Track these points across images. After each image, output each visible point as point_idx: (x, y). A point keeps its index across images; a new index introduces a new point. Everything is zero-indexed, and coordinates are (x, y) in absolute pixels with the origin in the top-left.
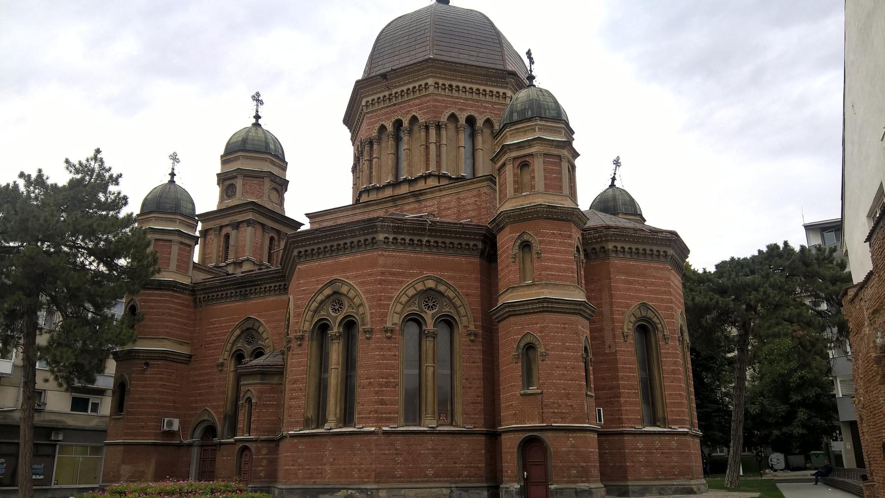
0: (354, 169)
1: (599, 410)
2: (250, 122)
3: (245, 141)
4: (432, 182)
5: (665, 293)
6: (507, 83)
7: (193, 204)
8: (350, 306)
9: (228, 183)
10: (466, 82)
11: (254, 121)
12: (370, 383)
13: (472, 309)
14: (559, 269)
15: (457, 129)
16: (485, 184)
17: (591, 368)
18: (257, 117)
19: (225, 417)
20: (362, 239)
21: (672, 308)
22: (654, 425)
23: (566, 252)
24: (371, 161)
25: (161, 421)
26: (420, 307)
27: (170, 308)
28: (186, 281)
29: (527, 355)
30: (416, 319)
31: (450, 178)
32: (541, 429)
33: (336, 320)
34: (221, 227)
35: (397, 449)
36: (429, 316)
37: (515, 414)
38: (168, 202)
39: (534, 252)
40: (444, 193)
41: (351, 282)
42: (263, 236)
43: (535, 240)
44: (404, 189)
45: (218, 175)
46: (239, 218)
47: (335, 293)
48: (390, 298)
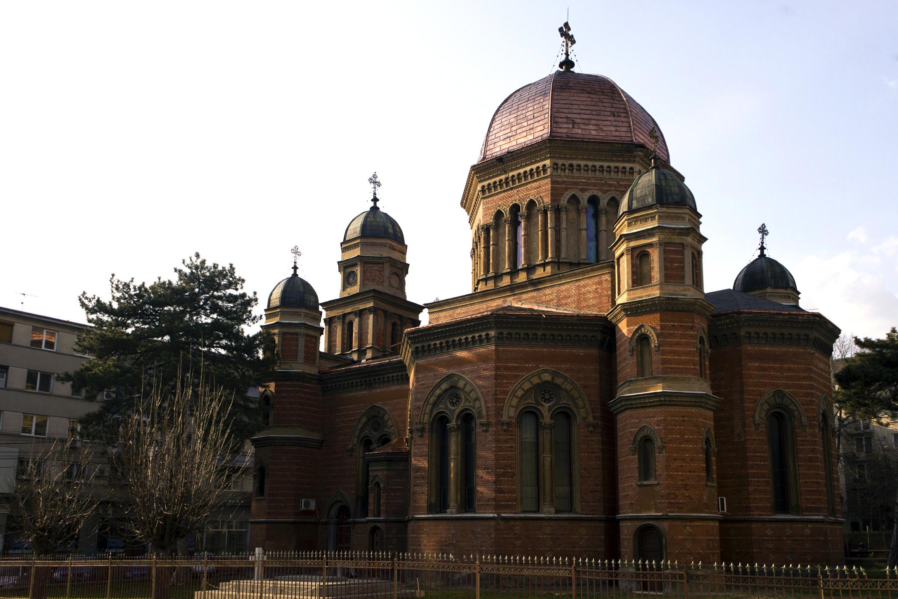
5: (805, 378)
8: (466, 400)
9: (349, 270)
11: (372, 204)
15: (578, 211)
17: (713, 459)
21: (812, 395)
23: (688, 344)
28: (313, 371)
30: (531, 413)
32: (657, 518)
33: (454, 412)
36: (545, 409)
37: (631, 504)
47: (452, 387)
48: (506, 393)
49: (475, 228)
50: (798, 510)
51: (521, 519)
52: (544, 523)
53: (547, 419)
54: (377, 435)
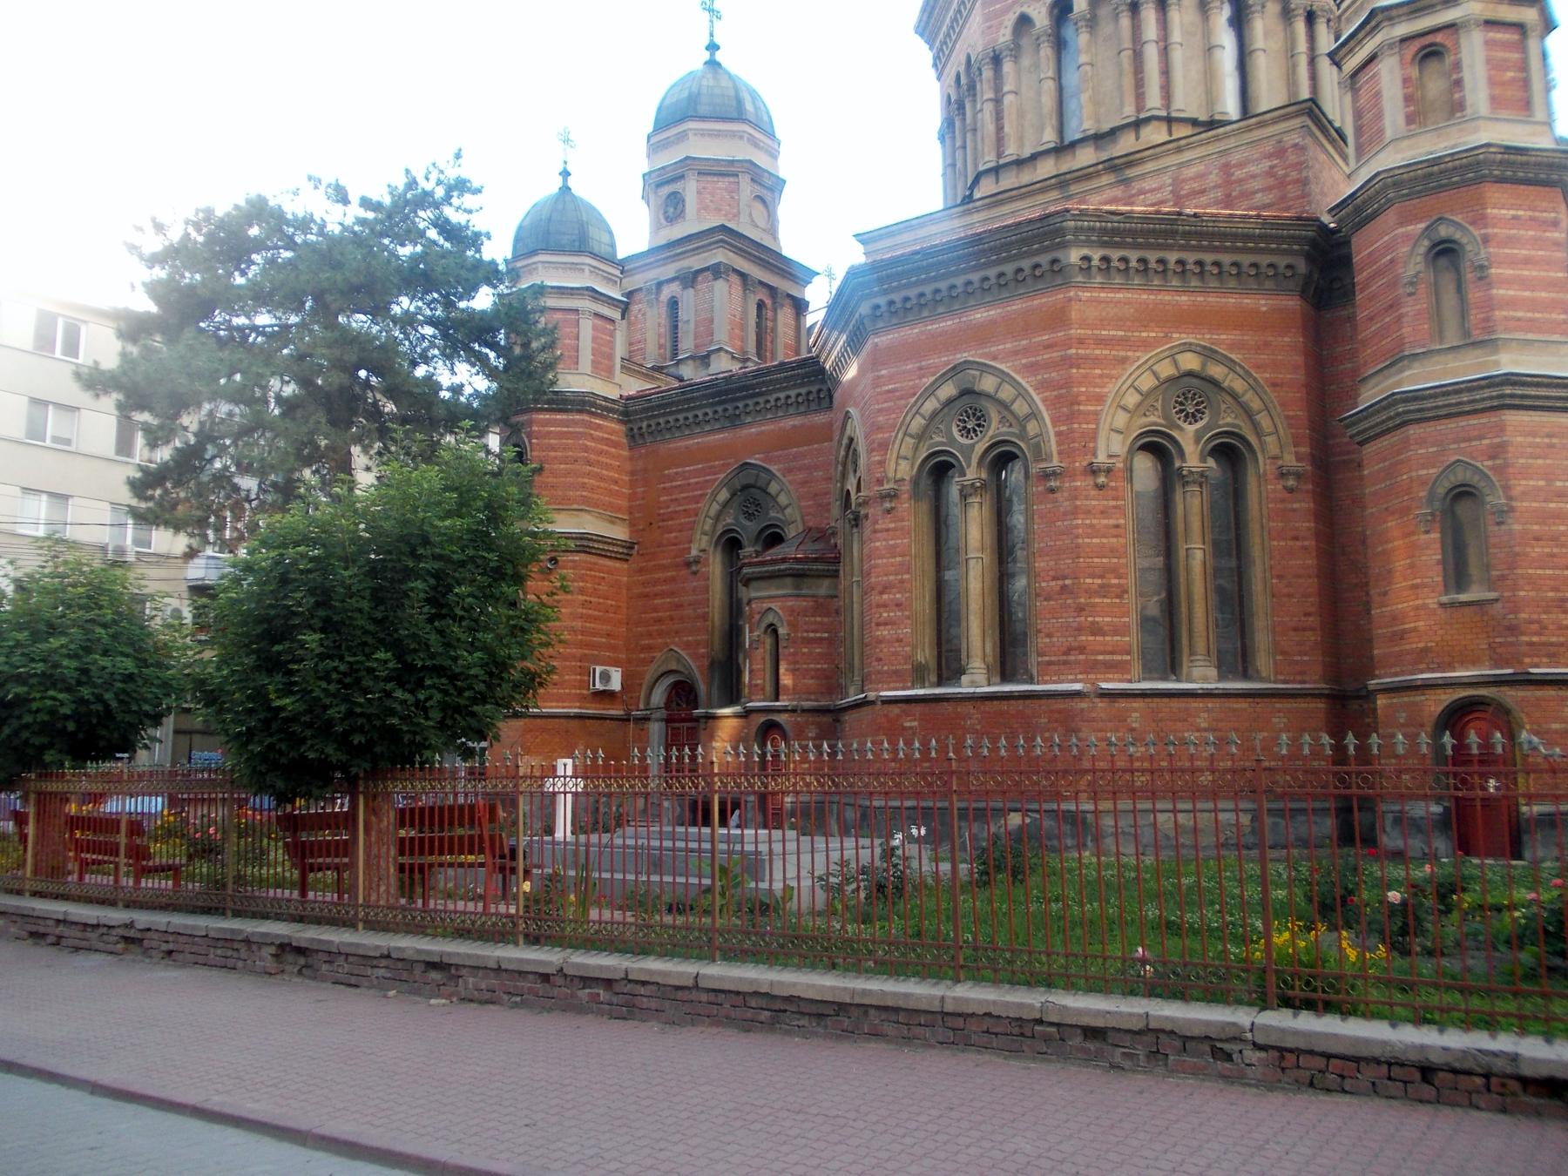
0: (948, 127)
3: (693, 99)
7: (610, 233)
8: (1003, 420)
9: (666, 190)
11: (706, 56)
12: (1064, 587)
14: (1534, 305)
16: (1297, 122)
19: (712, 664)
24: (998, 101)
25: (588, 673)
26: (1166, 417)
27: (586, 449)
28: (613, 394)
29: (1453, 513)
34: (660, 285)
35: (1133, 730)
38: (562, 229)
39: (1466, 266)
40: (1187, 156)
43: (1470, 237)
44: (1086, 157)
47: (967, 392)
49: (956, 64)
51: (1144, 695)
52: (1195, 704)
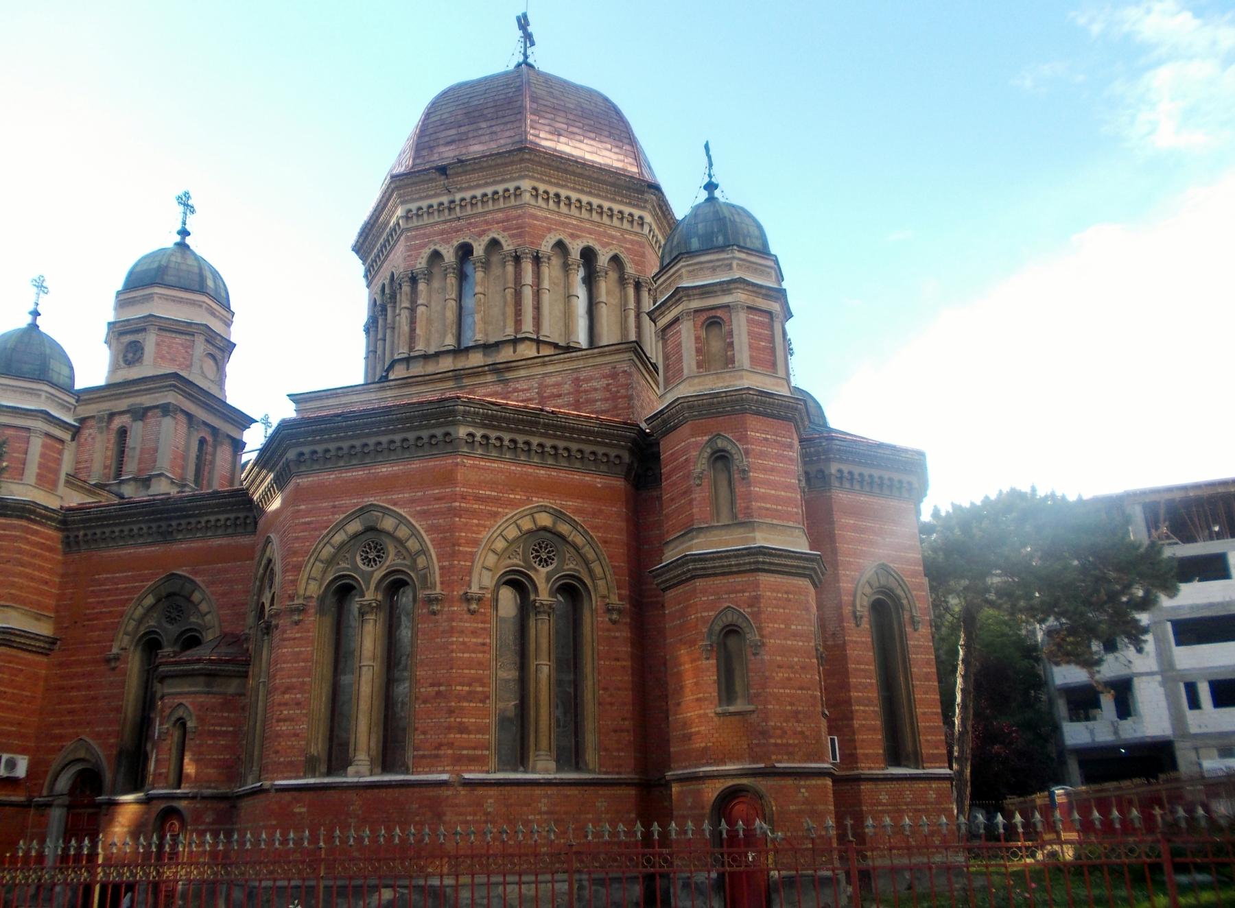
0: (371, 327)
1: (832, 741)
2: (171, 240)
4: (527, 350)
6: (646, 201)
7: (72, 368)
8: (398, 553)
9: (127, 339)
10: (582, 191)
11: (178, 239)
12: (438, 693)
13: (613, 567)
15: (566, 267)
16: (626, 356)
18: (184, 233)
19: (120, 754)
20: (397, 437)
22: (898, 764)
24: (413, 310)
27: (20, 551)
28: (54, 503)
31: (556, 346)
34: (112, 415)
36: (541, 577)
40: (550, 369)
41: (401, 511)
42: (189, 435)
44: (476, 359)
45: (109, 324)
46: (147, 400)
50: (917, 761)
52: (538, 791)
53: (544, 595)
54: (173, 630)
